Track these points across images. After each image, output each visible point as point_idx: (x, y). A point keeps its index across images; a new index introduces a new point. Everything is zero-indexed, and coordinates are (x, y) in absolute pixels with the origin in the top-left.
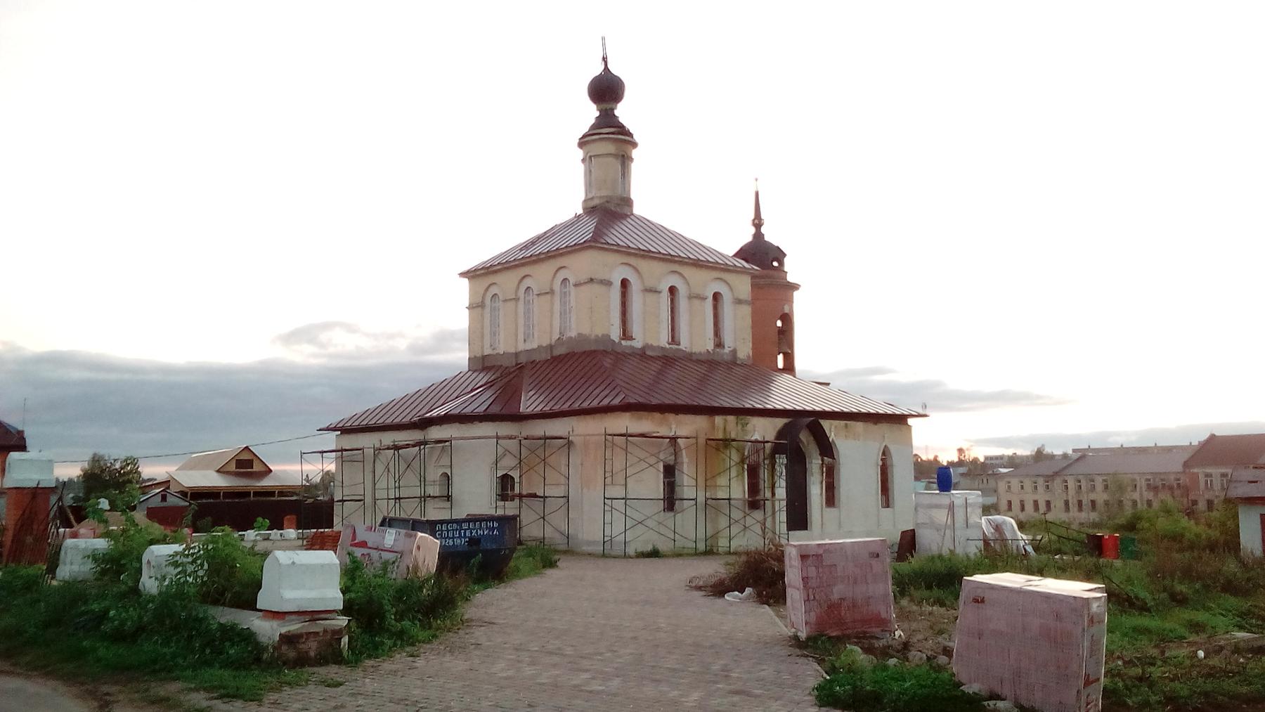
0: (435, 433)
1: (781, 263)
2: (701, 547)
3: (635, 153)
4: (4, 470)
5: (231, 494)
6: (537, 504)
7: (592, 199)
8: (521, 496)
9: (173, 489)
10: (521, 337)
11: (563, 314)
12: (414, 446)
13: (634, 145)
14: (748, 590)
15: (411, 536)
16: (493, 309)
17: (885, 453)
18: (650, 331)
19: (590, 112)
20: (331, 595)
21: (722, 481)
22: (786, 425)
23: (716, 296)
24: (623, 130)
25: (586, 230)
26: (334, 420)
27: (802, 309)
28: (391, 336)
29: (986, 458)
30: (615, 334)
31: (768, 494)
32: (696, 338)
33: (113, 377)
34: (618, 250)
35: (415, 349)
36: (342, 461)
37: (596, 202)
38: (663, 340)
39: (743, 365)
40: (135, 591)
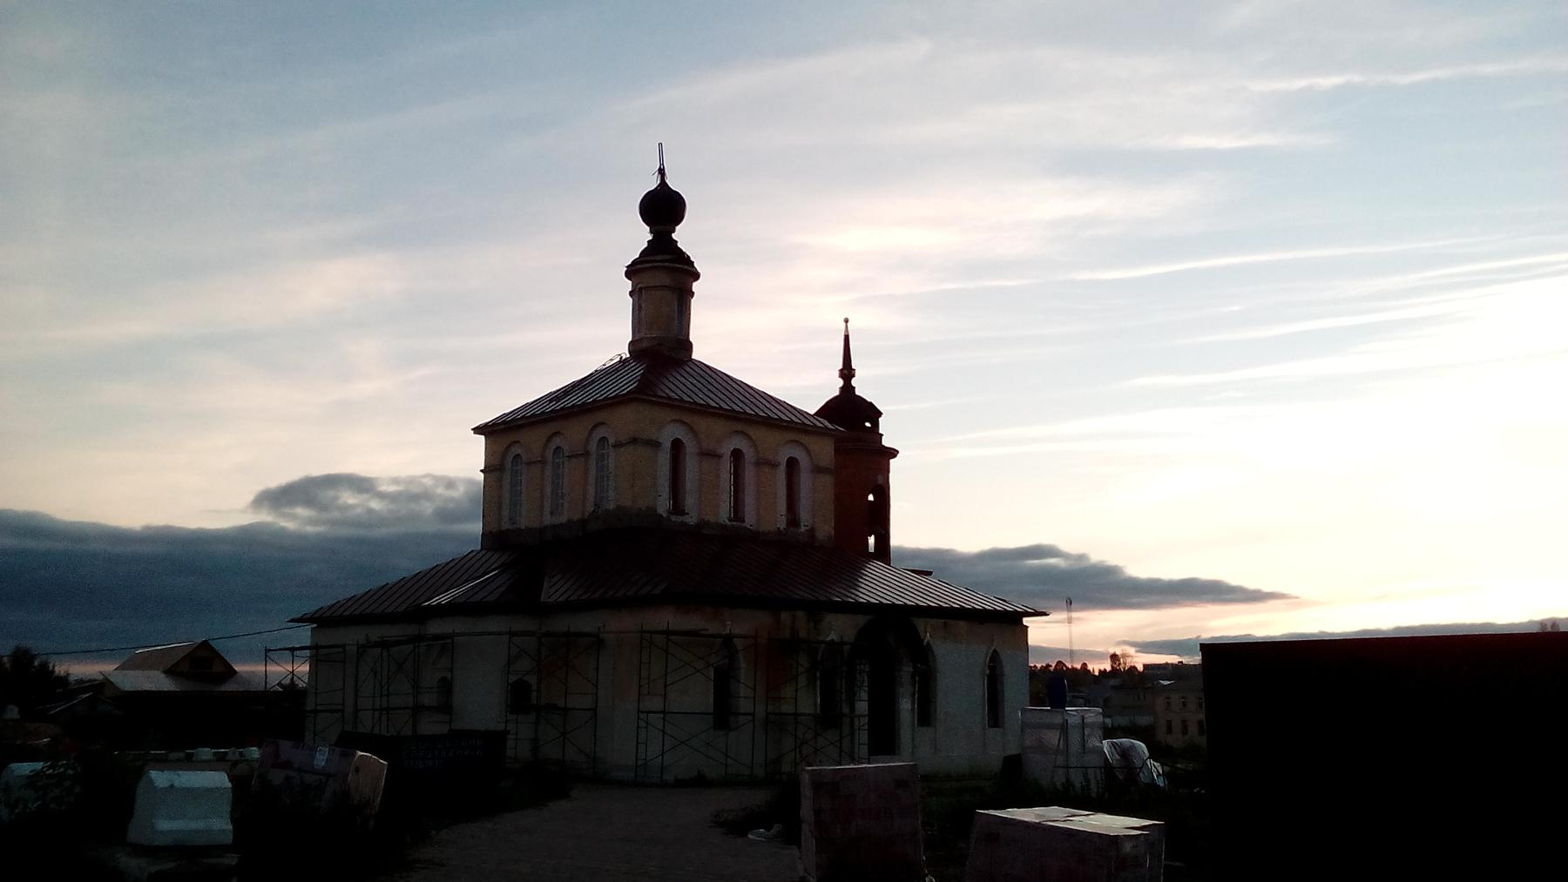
0: (436, 627)
1: (876, 425)
3: (696, 286)
7: (640, 340)
13: (696, 276)
14: (777, 828)
17: (995, 659)
18: (707, 500)
19: (641, 236)
21: (788, 691)
25: (627, 384)
26: (310, 607)
29: (1145, 666)
30: (663, 505)
31: (846, 710)
32: (765, 511)
33: (45, 545)
36: (315, 662)
37: (645, 344)
38: (724, 514)
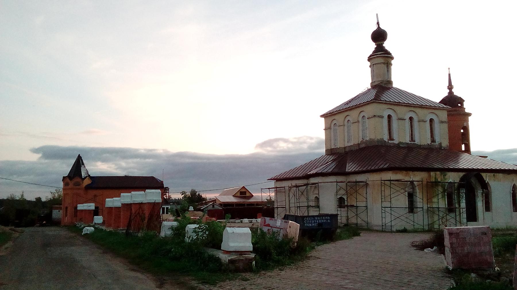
0: (312, 180)
1: (462, 104)
2: (426, 228)
4: (514, 191)
5: (238, 204)
6: (354, 210)
8: (347, 206)
9: (218, 203)
10: (346, 140)
11: (363, 130)
12: (304, 186)
13: (392, 58)
14: (435, 248)
15: (286, 222)
16: (334, 130)
18: (401, 136)
19: (372, 46)
20: (247, 245)
21: (435, 200)
22: (464, 175)
23: (431, 120)
24: (387, 53)
26: (273, 176)
27: (473, 124)
28: (301, 143)
30: (386, 138)
31: (457, 206)
32: (422, 138)
33: (200, 161)
34: (386, 103)
35: (310, 147)
36: (277, 192)
37: (376, 83)
38: (407, 140)
39: (444, 149)
40: (183, 241)
